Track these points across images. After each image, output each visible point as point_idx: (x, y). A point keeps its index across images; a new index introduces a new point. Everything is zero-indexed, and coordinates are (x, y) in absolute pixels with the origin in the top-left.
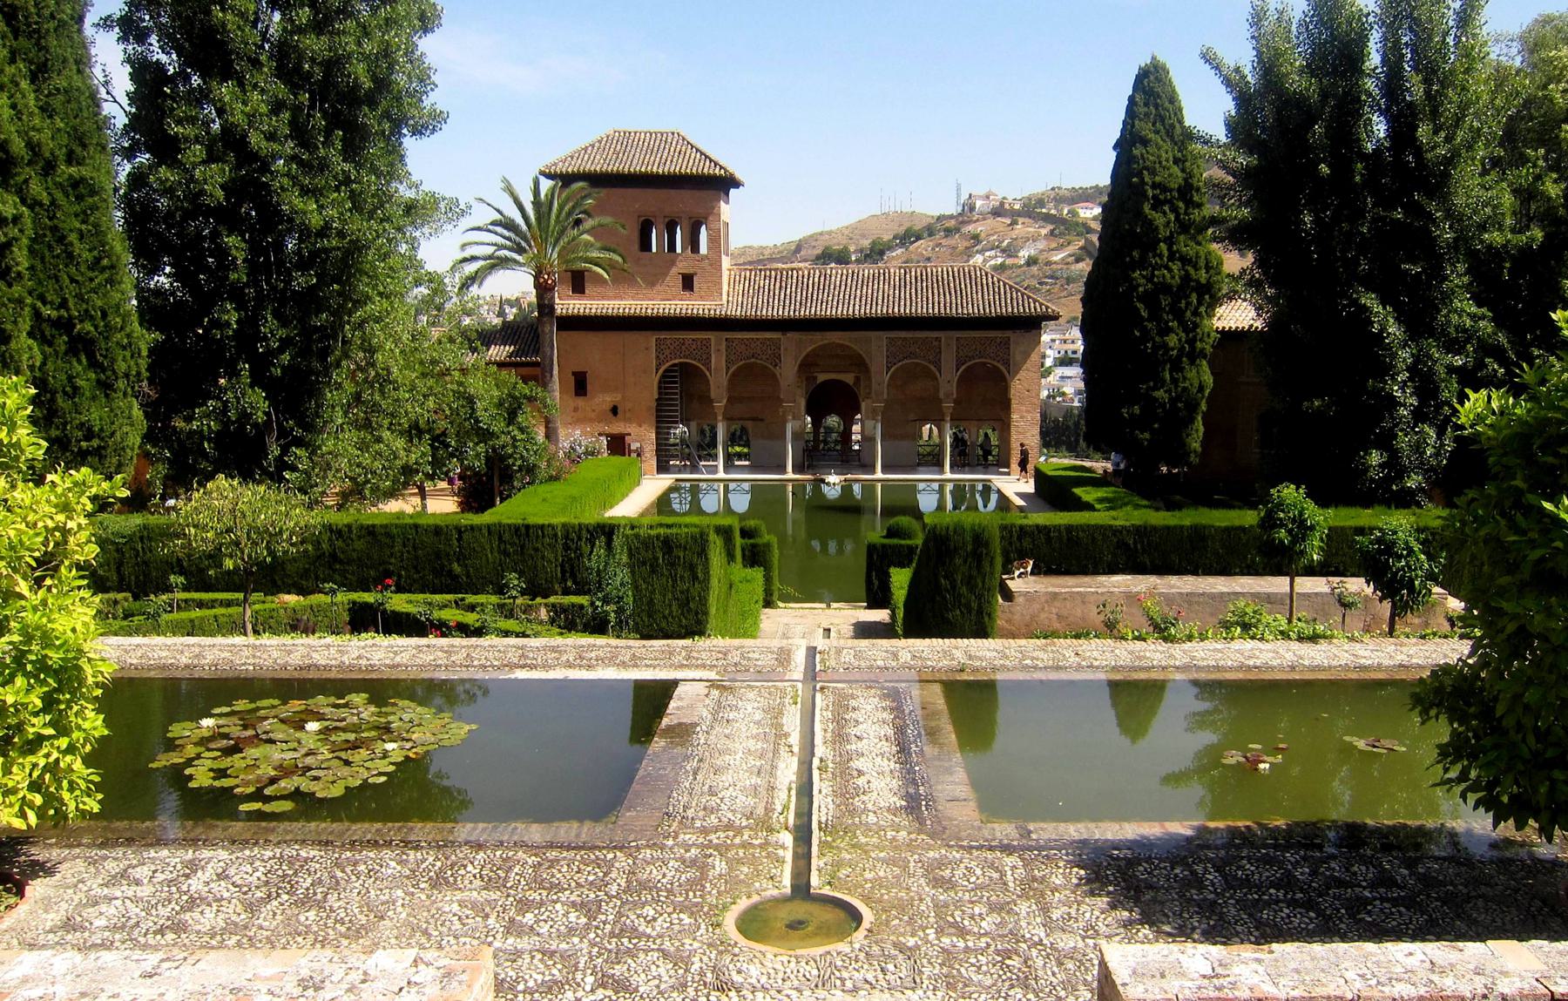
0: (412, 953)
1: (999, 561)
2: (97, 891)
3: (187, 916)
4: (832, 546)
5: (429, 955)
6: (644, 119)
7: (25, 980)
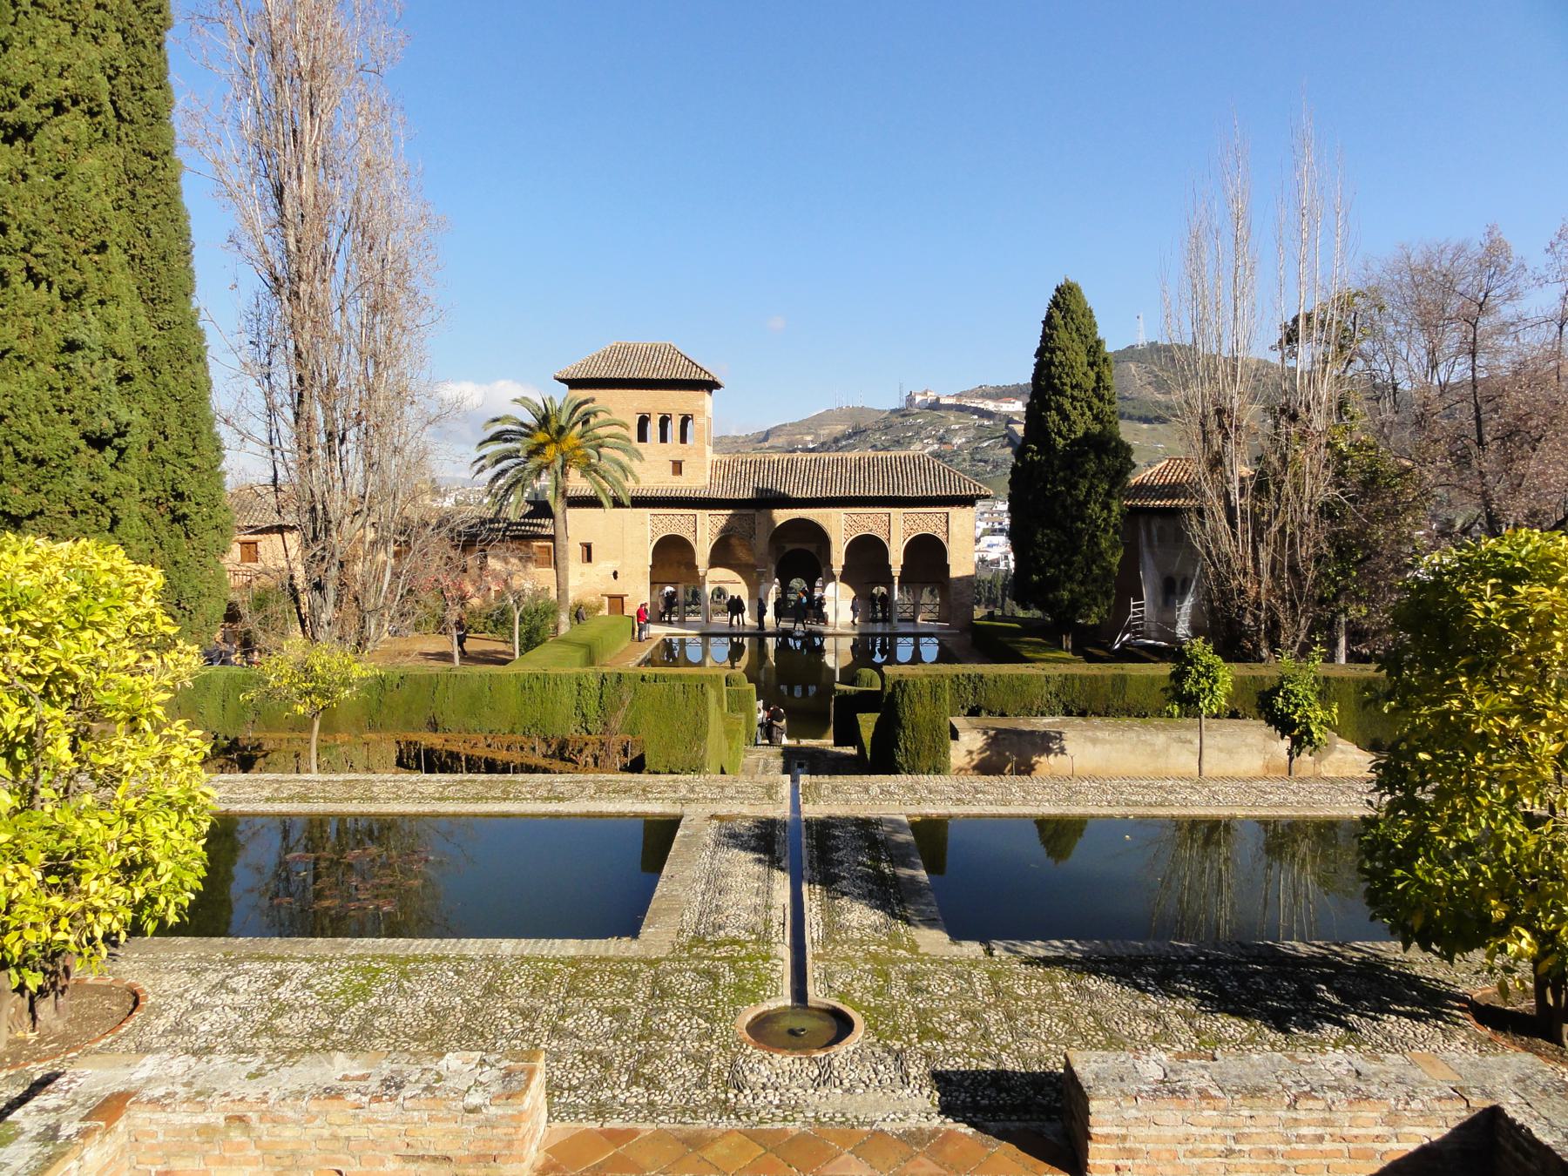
0: (477, 1055)
1: (947, 708)
2: (200, 1000)
3: (277, 1022)
4: (798, 691)
5: (492, 1058)
7: (149, 1080)
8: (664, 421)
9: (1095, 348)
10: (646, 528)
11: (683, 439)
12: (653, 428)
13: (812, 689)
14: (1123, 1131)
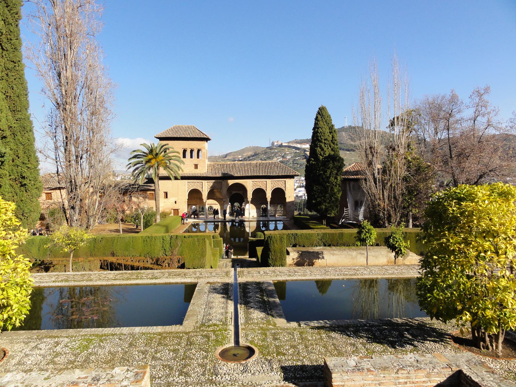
0: (126, 368)
2: (28, 353)
3: (56, 359)
5: (131, 369)
6: (184, 124)
8: (192, 151)
9: (331, 127)
10: (186, 186)
11: (198, 157)
12: (188, 154)
13: (242, 239)
14: (343, 383)
